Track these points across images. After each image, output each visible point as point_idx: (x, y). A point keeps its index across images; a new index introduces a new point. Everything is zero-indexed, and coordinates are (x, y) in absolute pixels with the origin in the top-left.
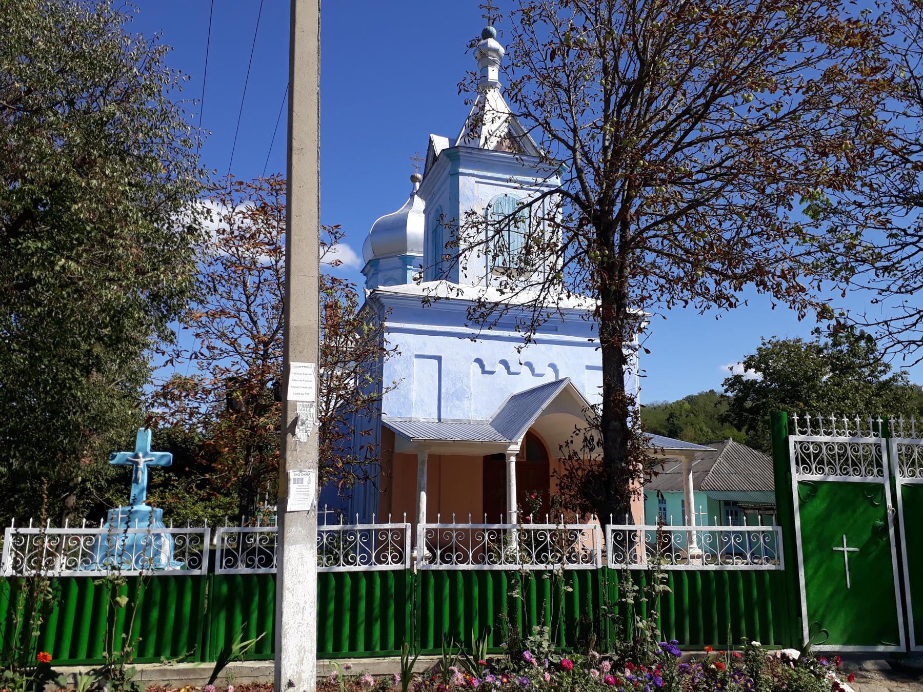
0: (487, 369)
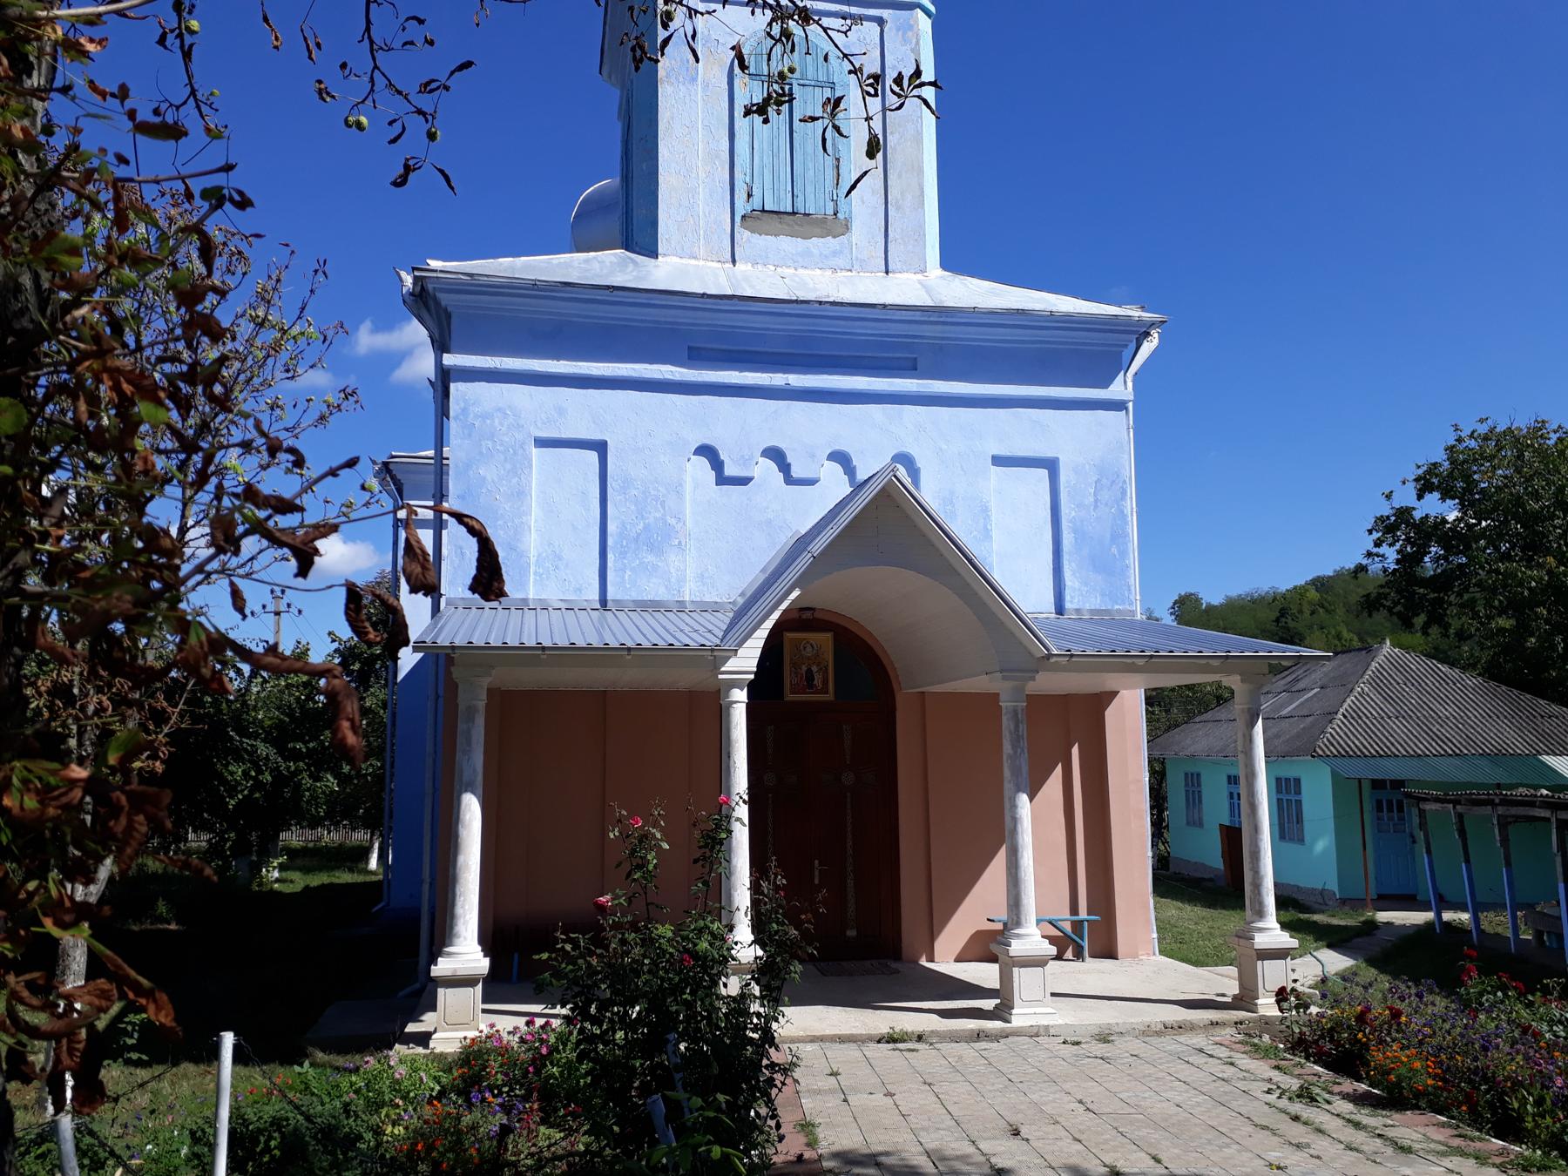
0: (729, 471)
